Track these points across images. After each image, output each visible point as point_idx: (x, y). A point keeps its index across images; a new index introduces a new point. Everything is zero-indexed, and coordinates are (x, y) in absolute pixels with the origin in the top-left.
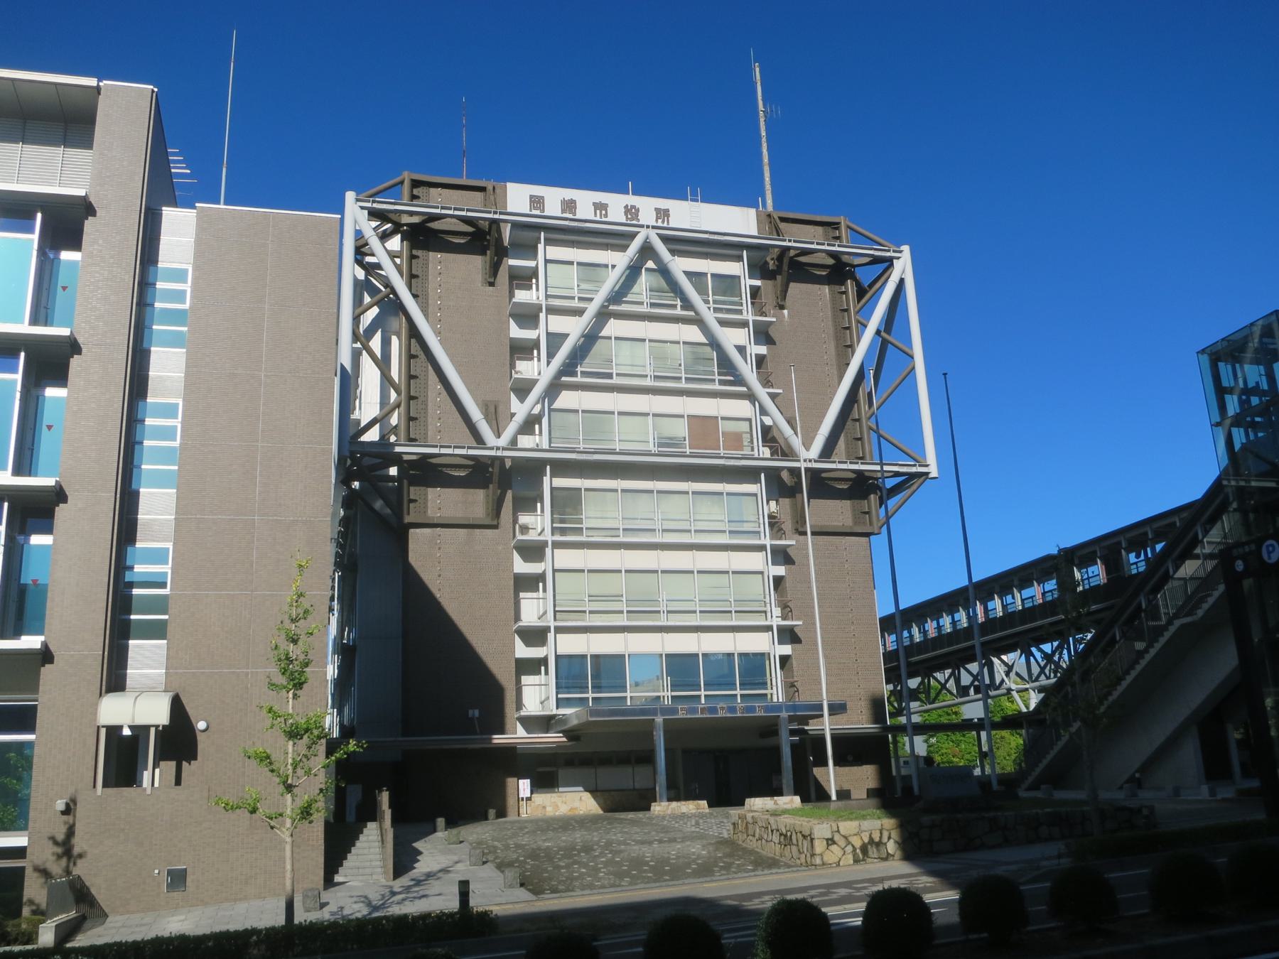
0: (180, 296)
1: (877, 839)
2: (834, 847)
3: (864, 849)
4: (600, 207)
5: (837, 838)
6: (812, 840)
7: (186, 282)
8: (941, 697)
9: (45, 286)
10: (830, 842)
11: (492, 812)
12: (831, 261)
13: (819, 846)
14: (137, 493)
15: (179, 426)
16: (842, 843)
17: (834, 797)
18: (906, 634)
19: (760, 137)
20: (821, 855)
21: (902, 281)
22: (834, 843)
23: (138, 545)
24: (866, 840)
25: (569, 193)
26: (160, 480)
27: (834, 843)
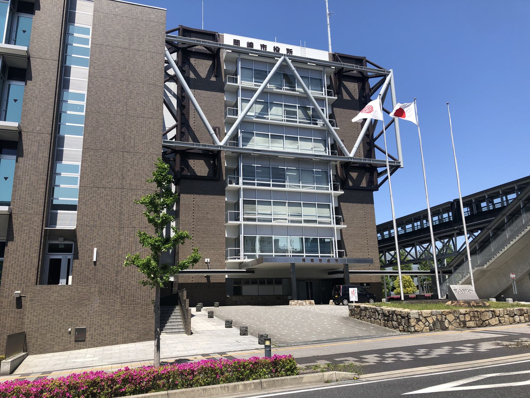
0: (85, 41)
1: (440, 320)
2: (420, 323)
3: (434, 324)
4: (263, 46)
5: (421, 318)
6: (409, 319)
7: (89, 35)
8: (432, 252)
9: (14, 28)
10: (418, 320)
11: (341, 304)
12: (360, 75)
13: (413, 322)
14: (63, 138)
15: (79, 177)
16: (424, 320)
17: (403, 298)
18: (425, 222)
19: (327, 25)
20: (414, 326)
21: (389, 84)
22: (421, 321)
23: (64, 162)
24: (435, 320)
25: (250, 40)
26: (74, 131)
27: (421, 321)
